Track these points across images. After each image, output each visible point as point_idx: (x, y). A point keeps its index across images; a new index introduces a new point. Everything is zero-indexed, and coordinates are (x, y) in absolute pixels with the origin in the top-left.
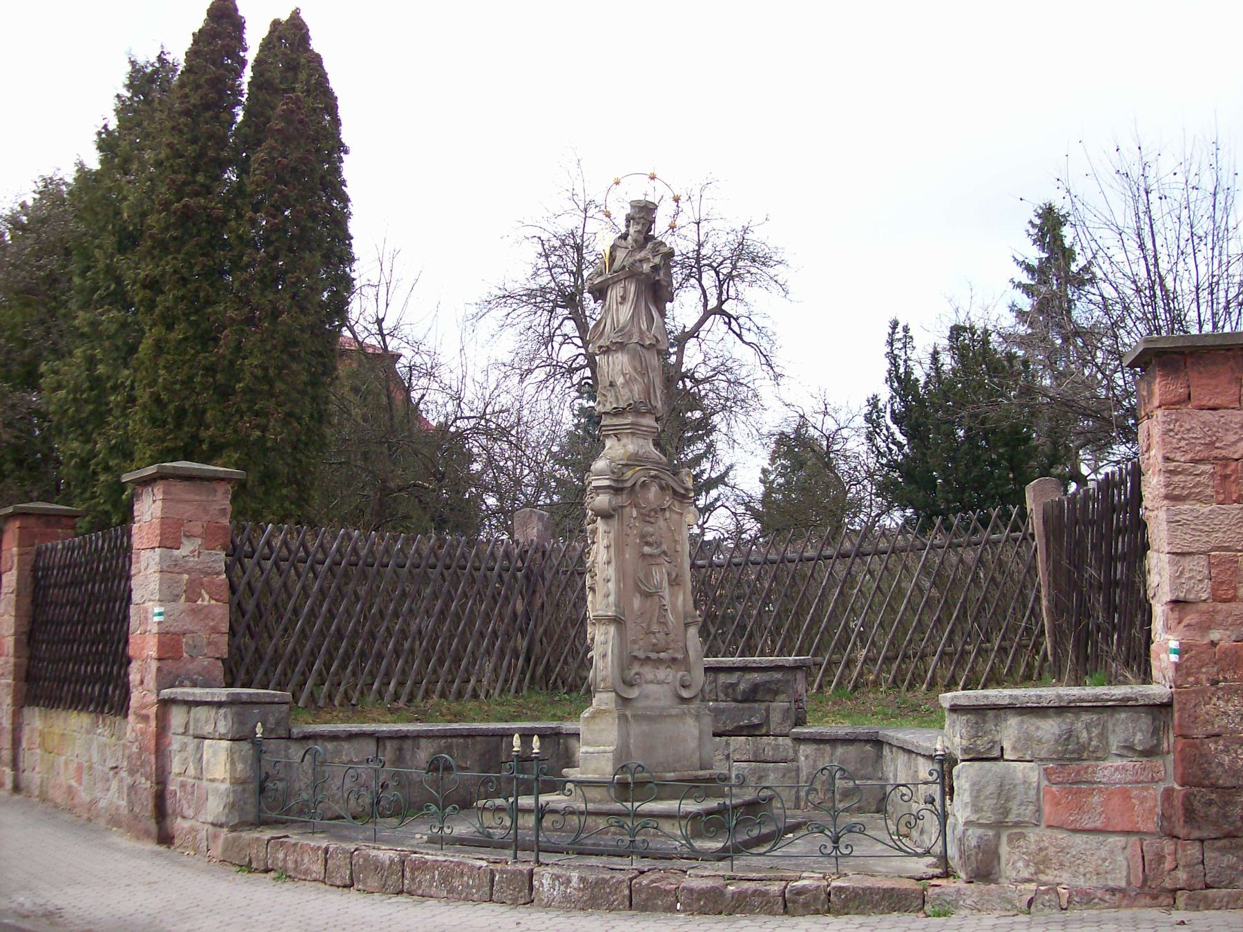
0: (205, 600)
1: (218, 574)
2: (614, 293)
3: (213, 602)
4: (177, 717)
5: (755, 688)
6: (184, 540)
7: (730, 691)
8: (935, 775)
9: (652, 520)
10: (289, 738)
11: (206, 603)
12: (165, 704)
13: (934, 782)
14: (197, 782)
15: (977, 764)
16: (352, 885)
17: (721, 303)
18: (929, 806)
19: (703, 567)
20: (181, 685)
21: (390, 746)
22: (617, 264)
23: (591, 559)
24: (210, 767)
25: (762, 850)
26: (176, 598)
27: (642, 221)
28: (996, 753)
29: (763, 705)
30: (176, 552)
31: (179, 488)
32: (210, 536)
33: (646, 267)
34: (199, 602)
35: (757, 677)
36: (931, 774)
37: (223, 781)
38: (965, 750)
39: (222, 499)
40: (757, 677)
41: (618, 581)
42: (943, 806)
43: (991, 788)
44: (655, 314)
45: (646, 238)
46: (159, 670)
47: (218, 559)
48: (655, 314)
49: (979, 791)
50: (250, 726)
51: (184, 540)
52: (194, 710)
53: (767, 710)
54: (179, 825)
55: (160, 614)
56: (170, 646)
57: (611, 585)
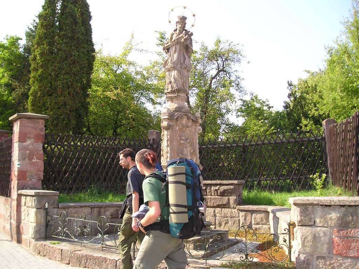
0: (35, 160)
1: (40, 151)
2: (173, 50)
3: (38, 160)
4: (23, 198)
5: (225, 191)
6: (27, 139)
7: (216, 192)
8: (287, 231)
9: (184, 131)
10: (58, 208)
11: (35, 161)
12: (20, 196)
13: (286, 234)
14: (28, 222)
15: (304, 228)
16: (69, 264)
17: (224, 68)
18: (285, 243)
19: (217, 148)
20: (26, 189)
21: (96, 210)
22: (173, 40)
23: (163, 145)
24: (30, 218)
25: (218, 258)
26: (25, 159)
27: (181, 23)
28: (312, 223)
29: (227, 197)
30: (24, 144)
31: (25, 121)
32: (37, 138)
33: (183, 40)
34: (33, 160)
35: (226, 187)
36: (285, 230)
37: (34, 222)
38: (299, 222)
39: (41, 124)
40: (226, 187)
41: (171, 154)
42: (290, 243)
43: (309, 238)
44: (186, 57)
45: (183, 28)
46: (18, 183)
47: (40, 146)
48: (186, 57)
49: (305, 239)
50: (43, 203)
51: (27, 139)
52: (27, 197)
53: (229, 199)
54: (24, 237)
55: (18, 165)
56: (22, 175)
57: (169, 155)
